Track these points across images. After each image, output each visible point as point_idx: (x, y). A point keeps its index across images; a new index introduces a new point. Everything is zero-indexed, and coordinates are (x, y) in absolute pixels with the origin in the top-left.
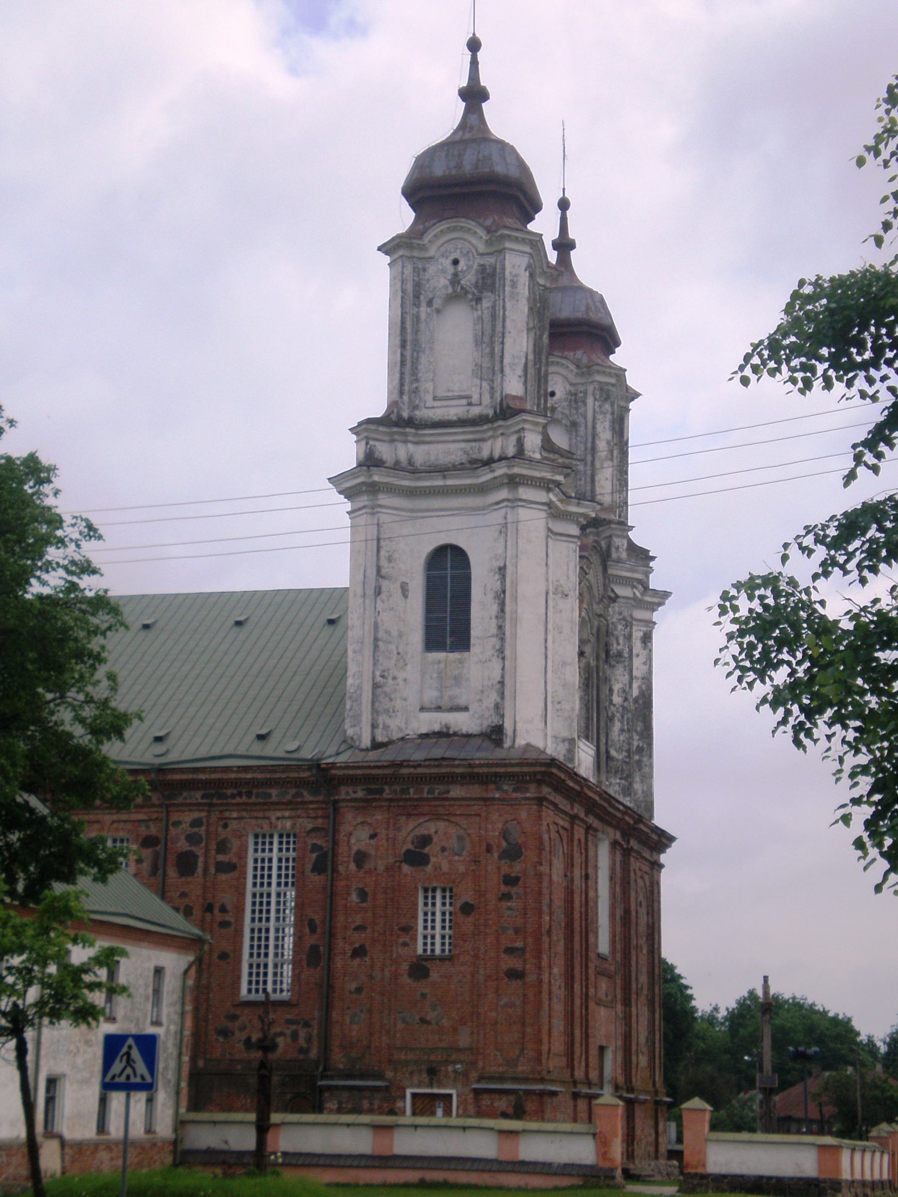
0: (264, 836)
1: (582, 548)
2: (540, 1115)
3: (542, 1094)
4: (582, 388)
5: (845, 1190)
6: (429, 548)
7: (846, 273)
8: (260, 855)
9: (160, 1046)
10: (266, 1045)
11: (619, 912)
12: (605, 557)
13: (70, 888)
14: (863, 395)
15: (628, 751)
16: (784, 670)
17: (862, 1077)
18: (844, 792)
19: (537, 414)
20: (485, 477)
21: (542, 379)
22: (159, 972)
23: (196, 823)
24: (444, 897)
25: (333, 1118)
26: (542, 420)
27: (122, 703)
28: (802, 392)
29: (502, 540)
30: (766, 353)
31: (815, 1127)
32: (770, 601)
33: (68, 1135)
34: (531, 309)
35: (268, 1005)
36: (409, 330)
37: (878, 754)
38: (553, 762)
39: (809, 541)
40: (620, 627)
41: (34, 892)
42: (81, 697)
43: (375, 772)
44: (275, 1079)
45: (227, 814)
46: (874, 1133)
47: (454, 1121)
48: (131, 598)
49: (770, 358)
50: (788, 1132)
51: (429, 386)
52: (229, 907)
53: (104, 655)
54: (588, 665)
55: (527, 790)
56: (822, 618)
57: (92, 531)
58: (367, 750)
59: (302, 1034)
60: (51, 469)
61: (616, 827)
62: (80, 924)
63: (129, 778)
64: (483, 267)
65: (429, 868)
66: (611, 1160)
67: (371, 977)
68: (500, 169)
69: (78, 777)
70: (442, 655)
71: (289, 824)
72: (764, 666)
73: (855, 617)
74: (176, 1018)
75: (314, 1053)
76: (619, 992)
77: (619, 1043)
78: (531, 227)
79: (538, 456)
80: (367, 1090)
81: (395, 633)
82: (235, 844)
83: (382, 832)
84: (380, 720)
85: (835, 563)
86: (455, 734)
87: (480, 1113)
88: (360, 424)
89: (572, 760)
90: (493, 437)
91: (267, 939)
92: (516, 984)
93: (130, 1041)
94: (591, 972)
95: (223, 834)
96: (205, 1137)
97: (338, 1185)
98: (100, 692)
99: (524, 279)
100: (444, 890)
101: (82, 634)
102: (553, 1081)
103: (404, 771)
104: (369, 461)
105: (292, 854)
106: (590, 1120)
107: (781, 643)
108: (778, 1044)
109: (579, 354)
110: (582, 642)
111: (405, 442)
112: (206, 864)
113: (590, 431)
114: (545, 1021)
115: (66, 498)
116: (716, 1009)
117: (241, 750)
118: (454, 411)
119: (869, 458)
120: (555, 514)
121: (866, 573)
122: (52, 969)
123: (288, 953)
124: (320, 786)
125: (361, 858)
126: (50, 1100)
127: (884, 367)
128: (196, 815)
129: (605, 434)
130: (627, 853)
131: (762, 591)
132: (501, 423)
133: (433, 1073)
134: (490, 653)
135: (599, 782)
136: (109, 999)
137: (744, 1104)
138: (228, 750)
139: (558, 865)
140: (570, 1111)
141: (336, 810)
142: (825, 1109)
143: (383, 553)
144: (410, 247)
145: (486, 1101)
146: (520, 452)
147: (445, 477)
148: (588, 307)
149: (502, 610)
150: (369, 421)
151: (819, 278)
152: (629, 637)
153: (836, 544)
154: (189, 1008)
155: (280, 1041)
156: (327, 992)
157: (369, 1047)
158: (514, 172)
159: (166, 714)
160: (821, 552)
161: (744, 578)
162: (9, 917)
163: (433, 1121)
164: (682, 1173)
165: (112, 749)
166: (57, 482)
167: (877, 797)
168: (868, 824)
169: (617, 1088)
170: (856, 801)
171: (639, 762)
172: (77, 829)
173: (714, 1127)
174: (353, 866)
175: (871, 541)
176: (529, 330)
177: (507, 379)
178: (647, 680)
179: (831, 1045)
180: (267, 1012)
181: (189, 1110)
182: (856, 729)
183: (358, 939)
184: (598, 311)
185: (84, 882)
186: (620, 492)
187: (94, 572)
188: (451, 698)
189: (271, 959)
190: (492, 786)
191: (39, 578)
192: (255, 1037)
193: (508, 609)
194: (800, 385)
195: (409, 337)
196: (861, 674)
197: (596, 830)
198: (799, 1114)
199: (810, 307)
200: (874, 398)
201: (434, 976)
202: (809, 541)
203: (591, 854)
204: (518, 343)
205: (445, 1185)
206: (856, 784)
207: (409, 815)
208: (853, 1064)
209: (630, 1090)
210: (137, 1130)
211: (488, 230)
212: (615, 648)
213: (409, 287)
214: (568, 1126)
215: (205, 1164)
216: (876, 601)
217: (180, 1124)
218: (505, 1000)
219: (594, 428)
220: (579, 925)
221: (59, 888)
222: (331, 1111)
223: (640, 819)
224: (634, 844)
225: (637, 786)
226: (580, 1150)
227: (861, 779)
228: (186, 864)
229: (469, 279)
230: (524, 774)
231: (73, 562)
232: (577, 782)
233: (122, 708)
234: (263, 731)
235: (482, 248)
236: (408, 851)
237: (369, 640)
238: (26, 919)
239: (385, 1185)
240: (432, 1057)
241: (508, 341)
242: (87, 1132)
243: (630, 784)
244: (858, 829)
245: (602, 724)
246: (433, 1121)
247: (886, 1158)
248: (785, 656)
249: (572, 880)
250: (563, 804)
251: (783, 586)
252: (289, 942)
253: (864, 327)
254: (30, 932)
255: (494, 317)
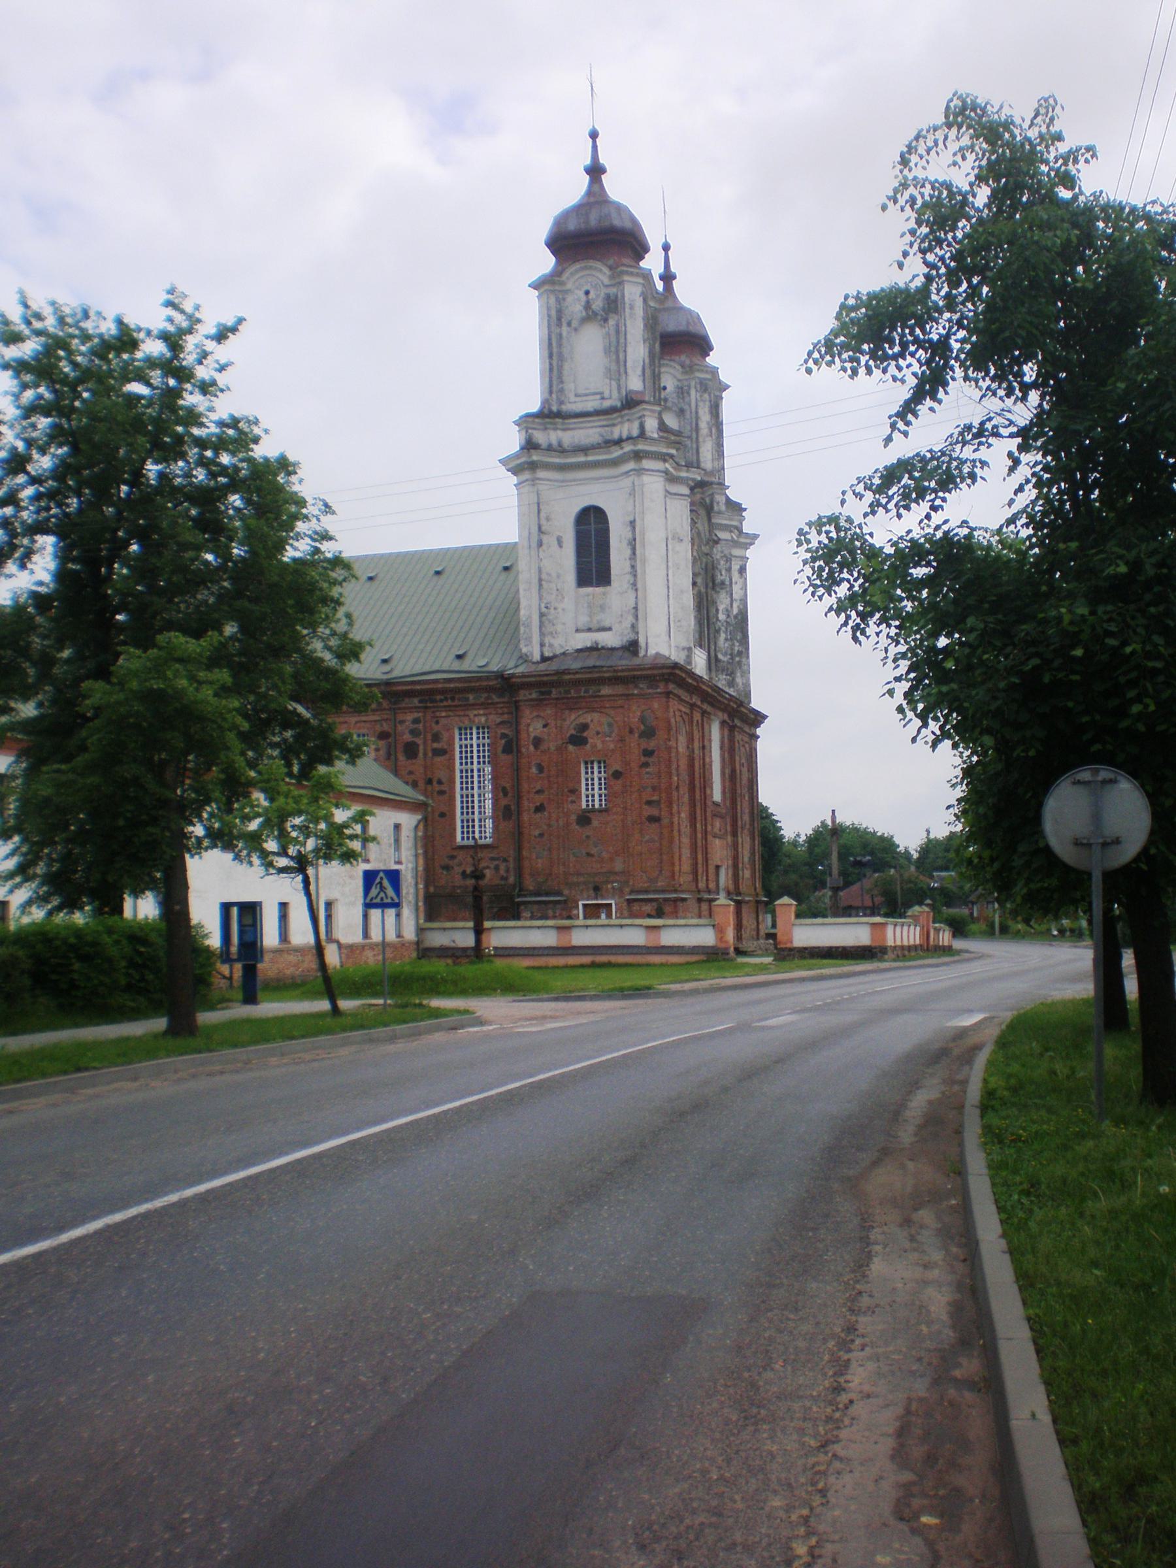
0: (466, 729)
1: (692, 504)
2: (675, 914)
3: (675, 900)
4: (686, 383)
5: (890, 953)
6: (577, 509)
7: (878, 289)
8: (464, 742)
9: (402, 877)
10: (478, 875)
11: (727, 771)
12: (709, 509)
13: (331, 769)
14: (894, 379)
15: (731, 655)
16: (845, 585)
17: (901, 875)
18: (890, 672)
19: (654, 404)
20: (616, 453)
21: (656, 377)
22: (397, 827)
23: (416, 721)
24: (600, 767)
25: (528, 923)
26: (658, 408)
27: (357, 635)
28: (851, 377)
29: (632, 501)
30: (823, 349)
31: (868, 912)
32: (834, 535)
33: (343, 940)
34: (645, 325)
35: (477, 847)
36: (554, 344)
37: (913, 644)
38: (676, 666)
39: (860, 488)
40: (722, 562)
41: (305, 773)
42: (328, 631)
43: (545, 679)
44: (485, 898)
45: (438, 714)
46: (909, 913)
47: (614, 921)
48: (358, 558)
49: (826, 353)
50: (850, 916)
51: (572, 386)
52: (444, 780)
53: (342, 600)
54: (700, 592)
55: (657, 687)
56: (871, 545)
57: (328, 508)
58: (538, 663)
59: (503, 867)
60: (294, 465)
61: (724, 710)
62: (340, 794)
63: (367, 690)
64: (608, 297)
65: (588, 746)
66: (726, 942)
67: (549, 826)
68: (617, 222)
69: (330, 690)
70: (590, 590)
71: (483, 719)
72: (831, 582)
73: (895, 544)
74: (412, 858)
75: (511, 880)
76: (729, 828)
77: (730, 862)
78: (642, 264)
79: (655, 435)
80: (553, 904)
81: (554, 575)
82: (445, 736)
83: (552, 723)
84: (547, 641)
85: (879, 504)
86: (603, 648)
87: (633, 915)
88: (521, 418)
89: (690, 663)
90: (622, 423)
91: (473, 802)
92: (654, 826)
93: (381, 874)
94: (709, 814)
95: (436, 728)
96: (438, 939)
97: (533, 968)
98: (341, 627)
99: (639, 303)
100: (599, 762)
101: (325, 585)
102: (683, 892)
103: (567, 677)
104: (530, 445)
105: (487, 741)
106: (710, 916)
107: (842, 565)
108: (842, 857)
109: (683, 358)
110: (694, 575)
111: (555, 429)
112: (425, 750)
113: (694, 415)
114: (676, 850)
115: (307, 485)
116: (798, 835)
117: (445, 667)
118: (591, 405)
119: (901, 425)
120: (671, 479)
121: (902, 511)
122: (322, 826)
123: (489, 810)
124: (502, 693)
125: (537, 742)
126: (329, 917)
127: (908, 357)
128: (416, 715)
129: (705, 417)
130: (732, 728)
131: (827, 528)
132: (626, 412)
133: (597, 890)
134: (626, 586)
135: (711, 678)
136: (364, 847)
137: (818, 900)
138: (436, 667)
139: (682, 739)
140: (696, 911)
141: (517, 708)
142: (876, 899)
143: (543, 515)
144: (553, 283)
145: (636, 907)
146: (642, 434)
147: (586, 455)
148: (688, 323)
149: (634, 554)
150: (528, 416)
151: (859, 292)
152: (729, 570)
153: (881, 489)
154: (420, 851)
155: (488, 872)
156: (519, 837)
157: (551, 874)
158: (628, 225)
159: (391, 643)
160: (869, 497)
161: (814, 518)
162: (290, 791)
163: (599, 922)
164: (776, 948)
165: (353, 669)
166: (301, 473)
167: (912, 675)
168: (906, 695)
169: (729, 893)
170: (898, 679)
171: (739, 663)
172: (331, 728)
173: (798, 916)
174: (532, 748)
175: (905, 487)
176: (644, 341)
177: (630, 378)
178: (744, 601)
179: (879, 855)
180: (476, 853)
181: (426, 921)
182: (896, 627)
183: (539, 799)
184: (695, 324)
185: (340, 765)
186: (718, 459)
187: (331, 538)
188: (598, 622)
189: (477, 816)
190: (631, 686)
191: (292, 545)
192: (469, 870)
193: (638, 552)
194: (849, 372)
195: (555, 350)
196: (900, 586)
197: (709, 713)
198: (857, 903)
199: (853, 315)
200: (903, 381)
201: (595, 823)
202: (860, 488)
203: (706, 731)
204: (637, 351)
205: (609, 965)
206: (898, 666)
207: (571, 709)
208: (895, 867)
209: (739, 894)
210: (391, 936)
211: (611, 268)
212: (719, 578)
213: (553, 313)
214: (695, 921)
215: (439, 957)
216: (909, 532)
217: (420, 930)
218: (647, 837)
219: (697, 413)
220: (698, 781)
221: (322, 769)
222: (526, 919)
223: (741, 704)
224: (737, 722)
225: (739, 680)
226: (705, 937)
227: (901, 662)
228: (411, 751)
229: (598, 305)
230: (655, 676)
231: (316, 533)
232: (695, 679)
233: (357, 638)
234: (461, 652)
235: (606, 281)
236: (572, 736)
237: (535, 581)
238: (302, 792)
239: (566, 966)
240: (596, 879)
241: (630, 350)
242: (356, 937)
243: (733, 679)
244: (899, 699)
245: (712, 636)
246: (599, 922)
247: (918, 929)
248: (845, 575)
249: (693, 751)
250: (685, 696)
251: (843, 523)
252: (489, 804)
253: (893, 328)
254: (305, 801)
255: (618, 332)
